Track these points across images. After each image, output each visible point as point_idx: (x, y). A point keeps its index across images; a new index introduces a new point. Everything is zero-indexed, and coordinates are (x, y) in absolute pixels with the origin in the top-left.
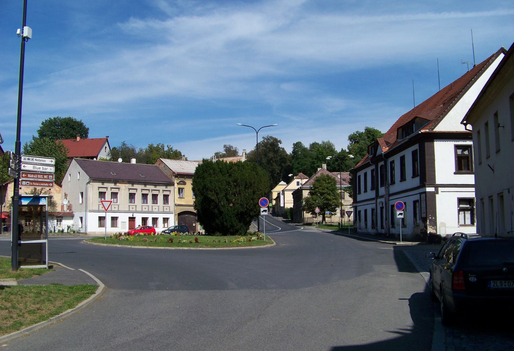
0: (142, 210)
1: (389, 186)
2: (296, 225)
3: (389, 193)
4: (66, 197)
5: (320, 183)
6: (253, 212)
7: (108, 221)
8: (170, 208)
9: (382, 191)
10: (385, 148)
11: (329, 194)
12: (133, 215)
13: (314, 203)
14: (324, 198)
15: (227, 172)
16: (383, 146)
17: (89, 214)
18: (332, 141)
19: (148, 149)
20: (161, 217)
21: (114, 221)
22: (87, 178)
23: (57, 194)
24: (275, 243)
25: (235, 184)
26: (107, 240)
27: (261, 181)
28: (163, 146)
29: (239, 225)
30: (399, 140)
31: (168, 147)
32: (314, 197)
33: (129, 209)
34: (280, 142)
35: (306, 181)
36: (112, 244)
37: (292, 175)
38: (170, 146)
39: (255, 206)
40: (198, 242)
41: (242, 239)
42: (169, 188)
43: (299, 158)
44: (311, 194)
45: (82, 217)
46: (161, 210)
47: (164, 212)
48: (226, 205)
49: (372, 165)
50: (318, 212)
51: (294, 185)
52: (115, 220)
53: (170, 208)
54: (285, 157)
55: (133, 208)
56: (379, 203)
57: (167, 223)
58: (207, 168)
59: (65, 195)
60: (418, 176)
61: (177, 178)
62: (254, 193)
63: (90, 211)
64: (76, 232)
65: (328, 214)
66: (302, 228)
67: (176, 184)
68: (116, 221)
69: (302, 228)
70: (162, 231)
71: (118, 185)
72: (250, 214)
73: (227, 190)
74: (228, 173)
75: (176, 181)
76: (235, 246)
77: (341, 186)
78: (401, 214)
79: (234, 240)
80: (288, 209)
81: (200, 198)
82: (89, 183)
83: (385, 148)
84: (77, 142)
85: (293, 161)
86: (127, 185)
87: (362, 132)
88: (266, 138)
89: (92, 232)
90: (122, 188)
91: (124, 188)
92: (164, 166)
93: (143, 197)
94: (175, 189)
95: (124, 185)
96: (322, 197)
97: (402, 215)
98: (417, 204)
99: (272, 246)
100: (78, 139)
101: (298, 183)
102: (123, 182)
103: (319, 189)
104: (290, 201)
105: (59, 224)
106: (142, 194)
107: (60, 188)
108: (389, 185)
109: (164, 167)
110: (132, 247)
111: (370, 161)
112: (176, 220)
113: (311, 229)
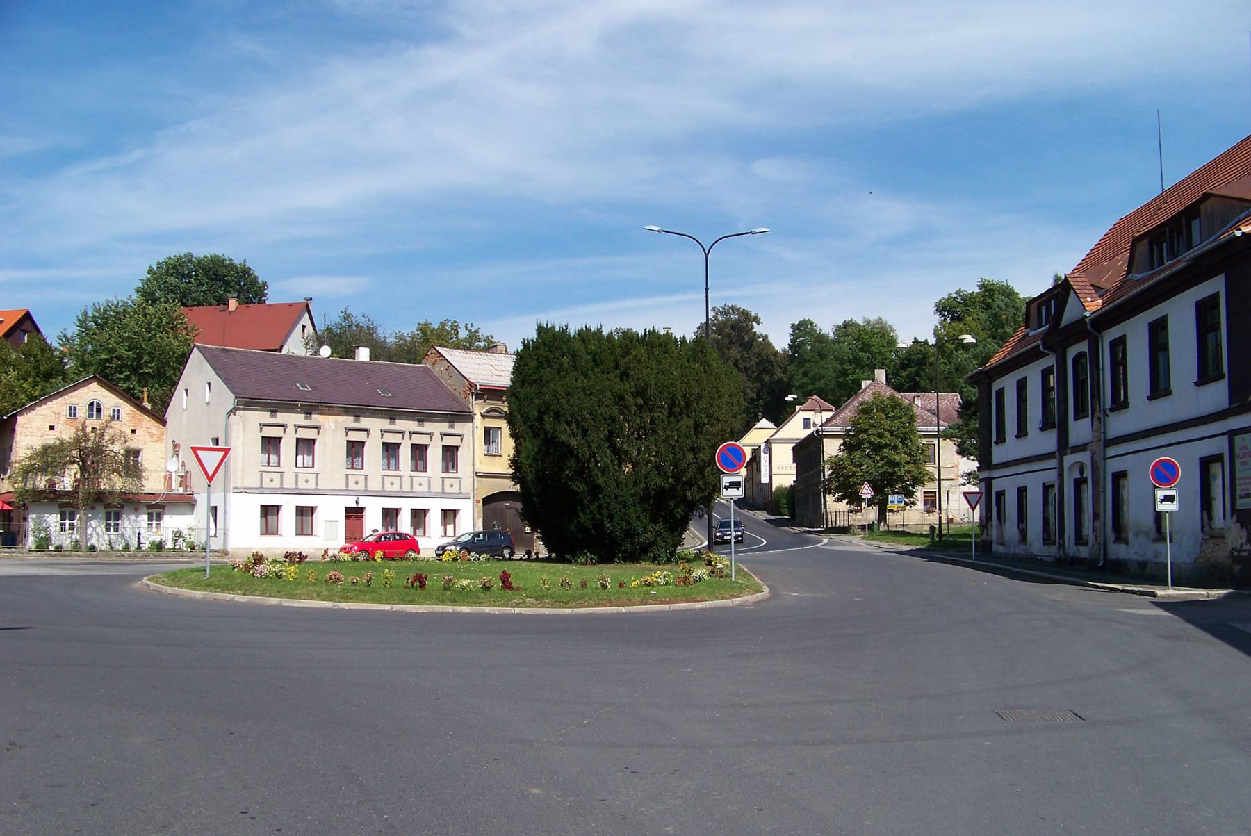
0: (383, 487)
1: (1106, 415)
2: (805, 532)
3: (1105, 438)
4: (175, 451)
5: (871, 418)
6: (695, 488)
7: (287, 519)
8: (460, 482)
9: (1080, 430)
10: (1092, 301)
11: (895, 448)
12: (357, 503)
13: (858, 472)
14: (882, 459)
15: (613, 364)
16: (1085, 296)
17: (234, 499)
18: (890, 319)
19: (418, 334)
20: (435, 508)
21: (304, 518)
22: (229, 399)
23: (152, 443)
24: (766, 590)
25: (640, 401)
26: (211, 576)
27: (718, 392)
28: (455, 326)
29: (650, 531)
30: (1137, 276)
31: (467, 329)
32: (857, 455)
33: (347, 485)
34: (756, 319)
35: (829, 417)
36: (223, 591)
37: (796, 397)
38: (472, 325)
39: (701, 470)
40: (510, 587)
41: (660, 574)
42: (459, 428)
43: (809, 361)
44: (847, 447)
45: (216, 507)
46: (436, 488)
47: (444, 493)
48: (611, 466)
49: (1046, 355)
50: (869, 496)
51: (795, 429)
52: (307, 516)
53: (460, 482)
54: (772, 357)
55: (357, 483)
56: (1070, 468)
57: (452, 525)
58: (550, 351)
59: (175, 446)
60: (1053, 426)
61: (482, 401)
62: (697, 428)
63: (235, 491)
64: (197, 548)
65: (896, 502)
66: (825, 541)
67: (478, 418)
68: (310, 518)
69: (825, 541)
70: (437, 548)
71: (317, 419)
72: (686, 496)
73: (614, 420)
74: (617, 367)
75: (478, 409)
76: (638, 599)
77: (938, 429)
78: (1169, 498)
79: (633, 581)
80: (779, 489)
81: (531, 446)
82: (233, 411)
83: (1092, 301)
84: (230, 312)
85: (792, 367)
86: (341, 419)
87: (970, 292)
88: (721, 310)
89: (243, 549)
90: (327, 427)
91: (332, 428)
92: (447, 368)
93: (387, 451)
94: (476, 429)
95: (332, 418)
96: (878, 458)
97: (1172, 502)
98: (1216, 469)
99: (760, 598)
100: (233, 304)
101: (807, 423)
102: (330, 409)
103: (869, 435)
104: (784, 469)
105: (154, 526)
106: (384, 444)
107: (161, 427)
108: (1107, 412)
109: (446, 370)
110: (284, 604)
111: (1040, 342)
112: (479, 517)
113: (851, 544)
